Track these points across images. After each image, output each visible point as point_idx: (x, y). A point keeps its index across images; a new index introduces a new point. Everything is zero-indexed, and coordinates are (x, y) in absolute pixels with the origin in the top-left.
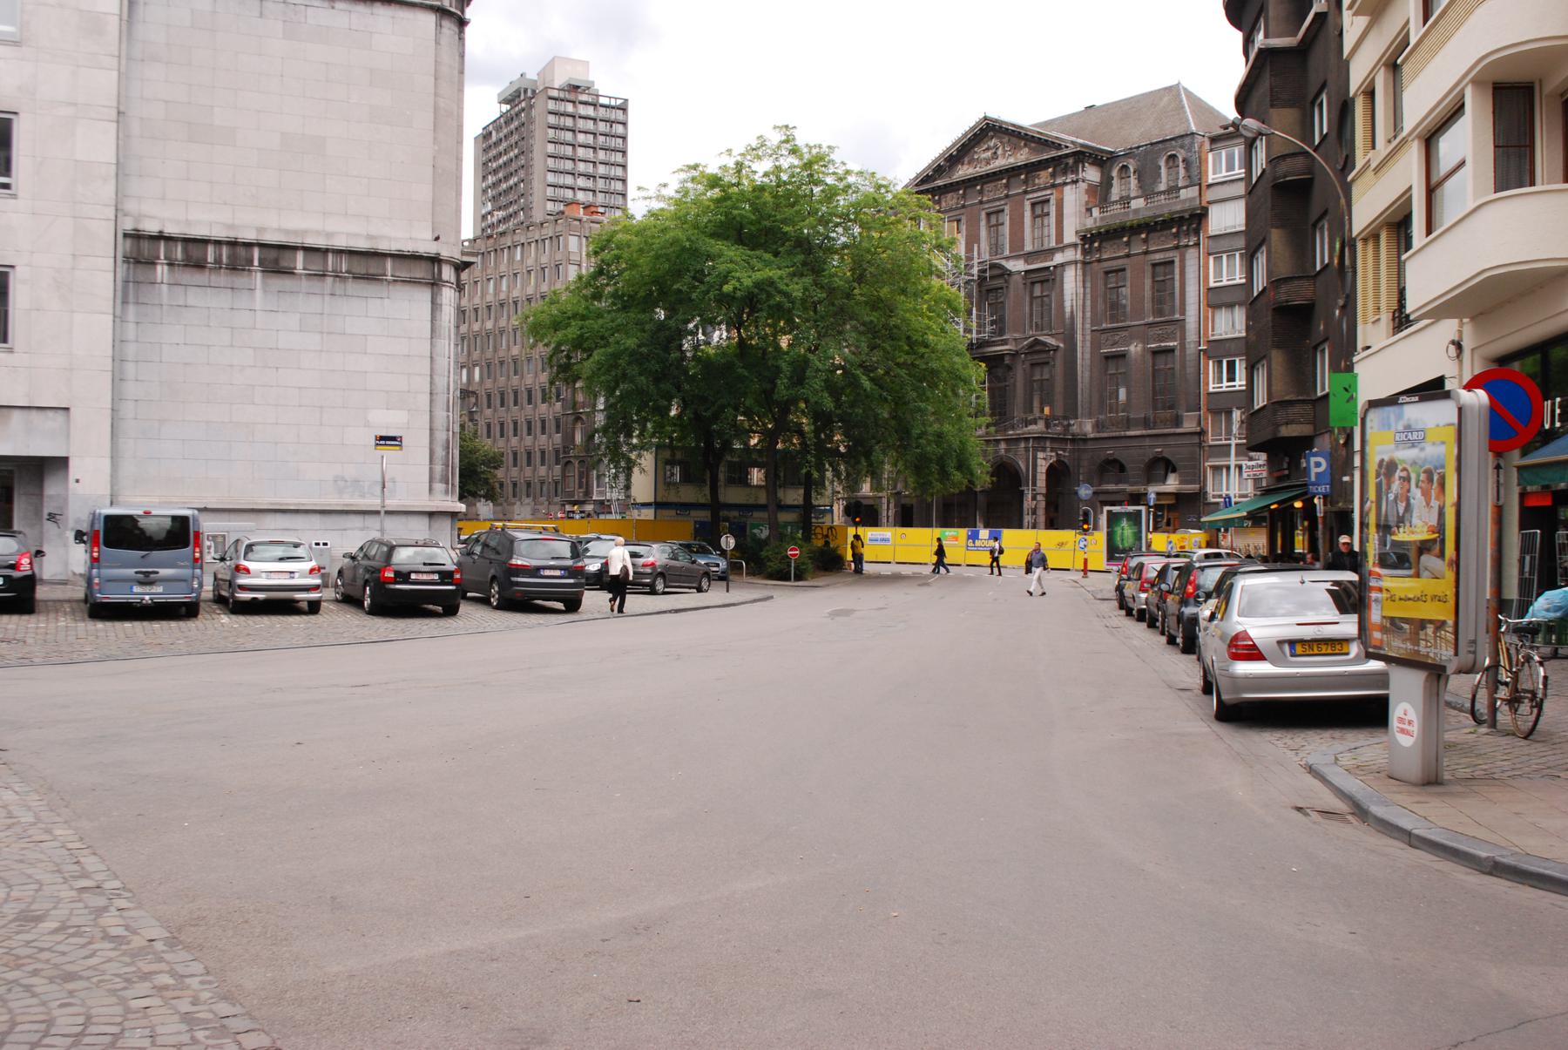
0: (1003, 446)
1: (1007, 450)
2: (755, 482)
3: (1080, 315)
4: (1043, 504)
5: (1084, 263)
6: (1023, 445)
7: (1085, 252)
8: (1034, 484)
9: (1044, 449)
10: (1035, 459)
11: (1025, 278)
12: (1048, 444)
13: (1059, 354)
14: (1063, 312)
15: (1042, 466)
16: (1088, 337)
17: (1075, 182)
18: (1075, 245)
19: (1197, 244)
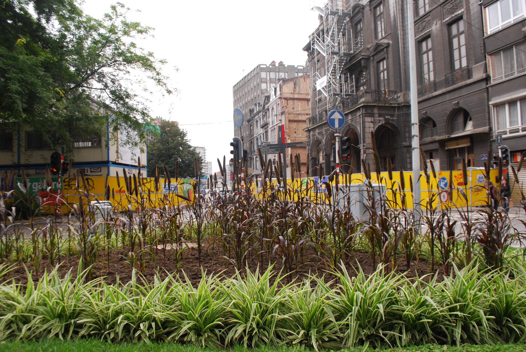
8: (364, 142)
9: (372, 115)
10: (364, 122)
13: (390, 49)
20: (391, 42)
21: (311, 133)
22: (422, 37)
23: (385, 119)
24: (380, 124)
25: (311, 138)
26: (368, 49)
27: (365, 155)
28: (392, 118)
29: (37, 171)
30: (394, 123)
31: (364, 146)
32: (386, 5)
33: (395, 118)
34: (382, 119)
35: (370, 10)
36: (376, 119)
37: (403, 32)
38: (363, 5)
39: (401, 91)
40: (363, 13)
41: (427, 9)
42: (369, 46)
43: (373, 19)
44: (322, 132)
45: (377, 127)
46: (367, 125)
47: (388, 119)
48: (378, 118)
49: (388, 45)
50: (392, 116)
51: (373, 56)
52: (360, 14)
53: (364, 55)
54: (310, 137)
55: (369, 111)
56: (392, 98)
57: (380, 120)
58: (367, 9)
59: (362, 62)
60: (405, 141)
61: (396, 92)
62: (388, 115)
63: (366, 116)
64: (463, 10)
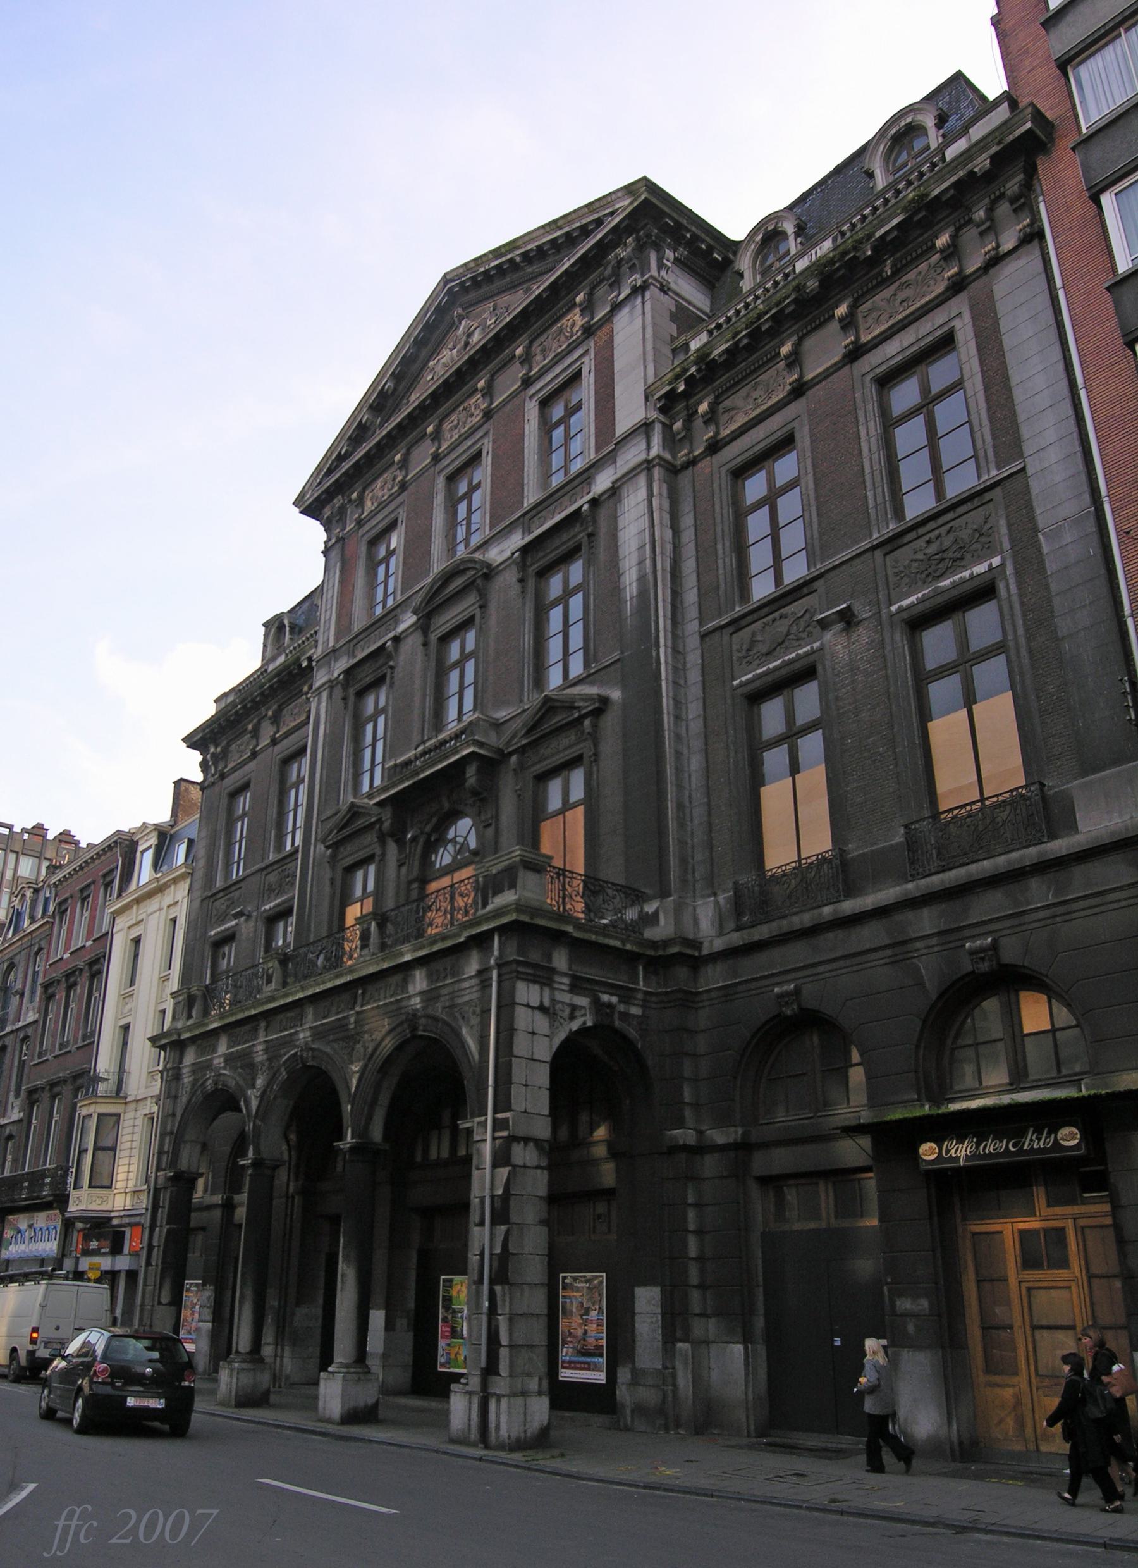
0: (419, 982)
1: (429, 996)
2: (898, 1303)
3: (663, 594)
4: (537, 1183)
5: (673, 471)
6: (473, 966)
7: (671, 441)
8: (503, 1103)
9: (543, 976)
10: (507, 1005)
11: (522, 565)
12: (560, 960)
13: (610, 722)
14: (616, 590)
15: (538, 1042)
16: (694, 658)
17: (639, 290)
18: (645, 427)
19: (1034, 236)
20: (616, 695)
21: (190, 1057)
22: (769, 678)
23: (597, 1004)
24: (575, 1026)
25: (187, 1079)
26: (497, 725)
27: (503, 1172)
28: (622, 1008)
29: (282, 1175)
30: (633, 1033)
31: (498, 1125)
32: (602, 555)
33: (635, 1011)
34: (583, 1001)
35: (521, 581)
36: (559, 996)
37: (674, 658)
38: (489, 566)
39: (664, 894)
40: (483, 595)
41: (796, 571)
42: (502, 714)
43: (529, 615)
44: (248, 1054)
45: (562, 1036)
46: (522, 1018)
47: (610, 1005)
48: (566, 998)
49: (602, 705)
50: (627, 996)
51: (522, 750)
52: (472, 599)
53: (481, 745)
54: (177, 1077)
55: (535, 956)
56: (613, 924)
57: (574, 1008)
58: (510, 577)
59: (471, 771)
60: (680, 1123)
61: (636, 897)
62: (613, 989)
63: (520, 976)
64: (996, 561)
